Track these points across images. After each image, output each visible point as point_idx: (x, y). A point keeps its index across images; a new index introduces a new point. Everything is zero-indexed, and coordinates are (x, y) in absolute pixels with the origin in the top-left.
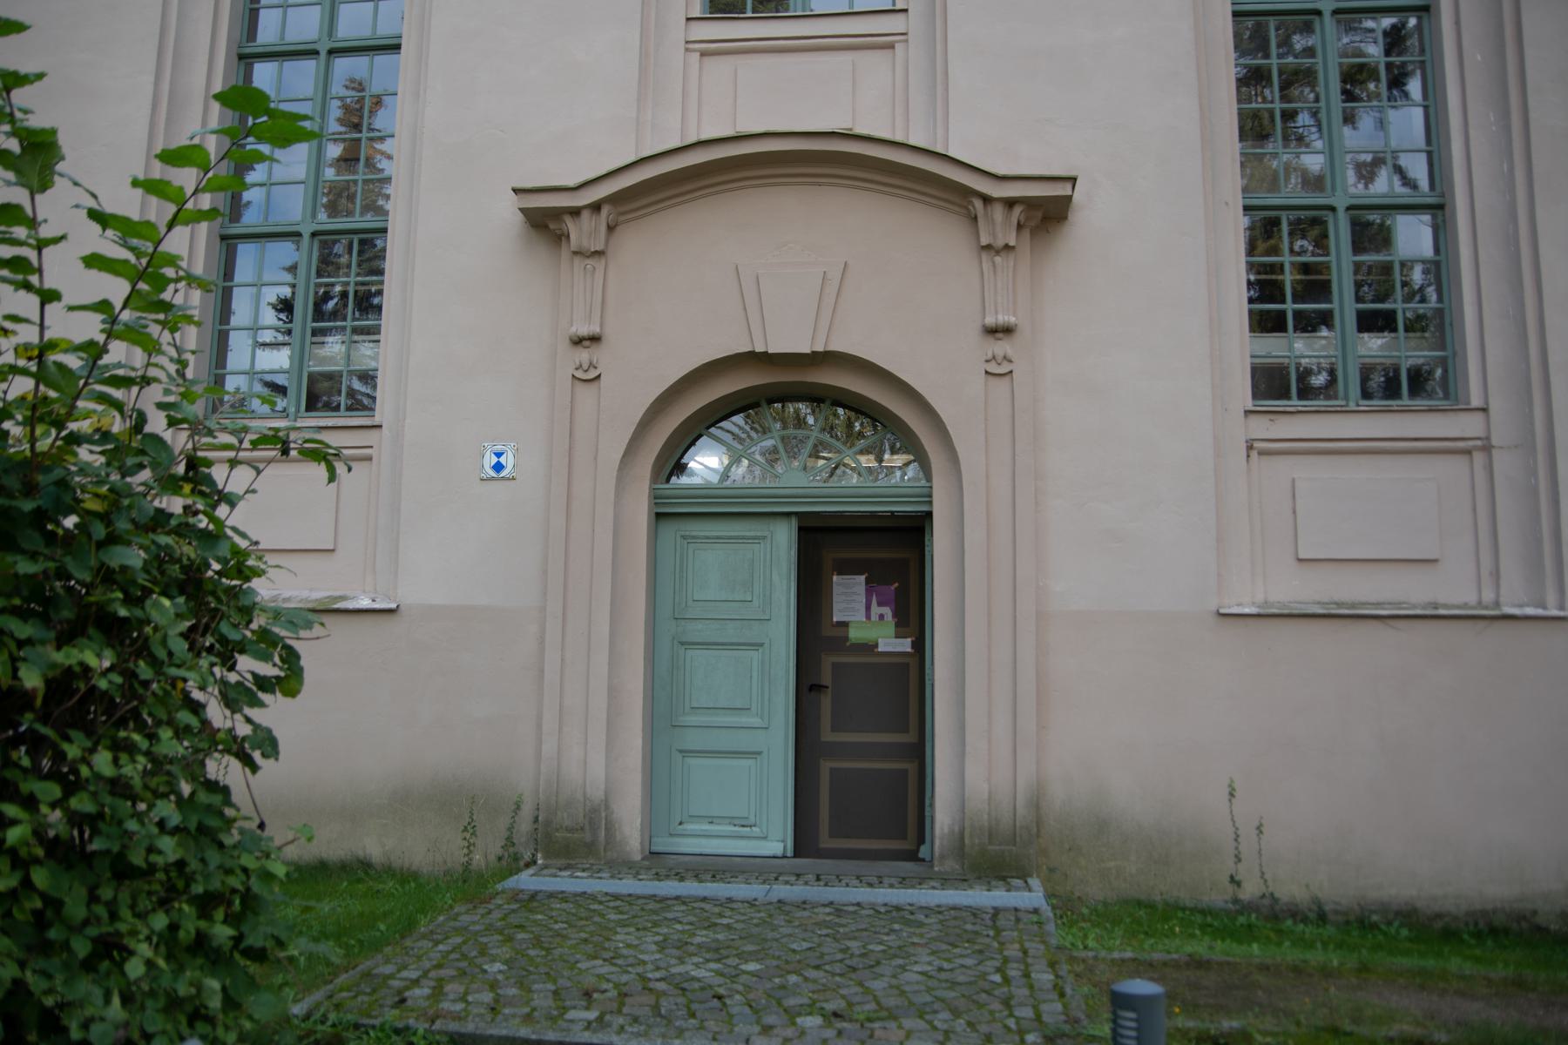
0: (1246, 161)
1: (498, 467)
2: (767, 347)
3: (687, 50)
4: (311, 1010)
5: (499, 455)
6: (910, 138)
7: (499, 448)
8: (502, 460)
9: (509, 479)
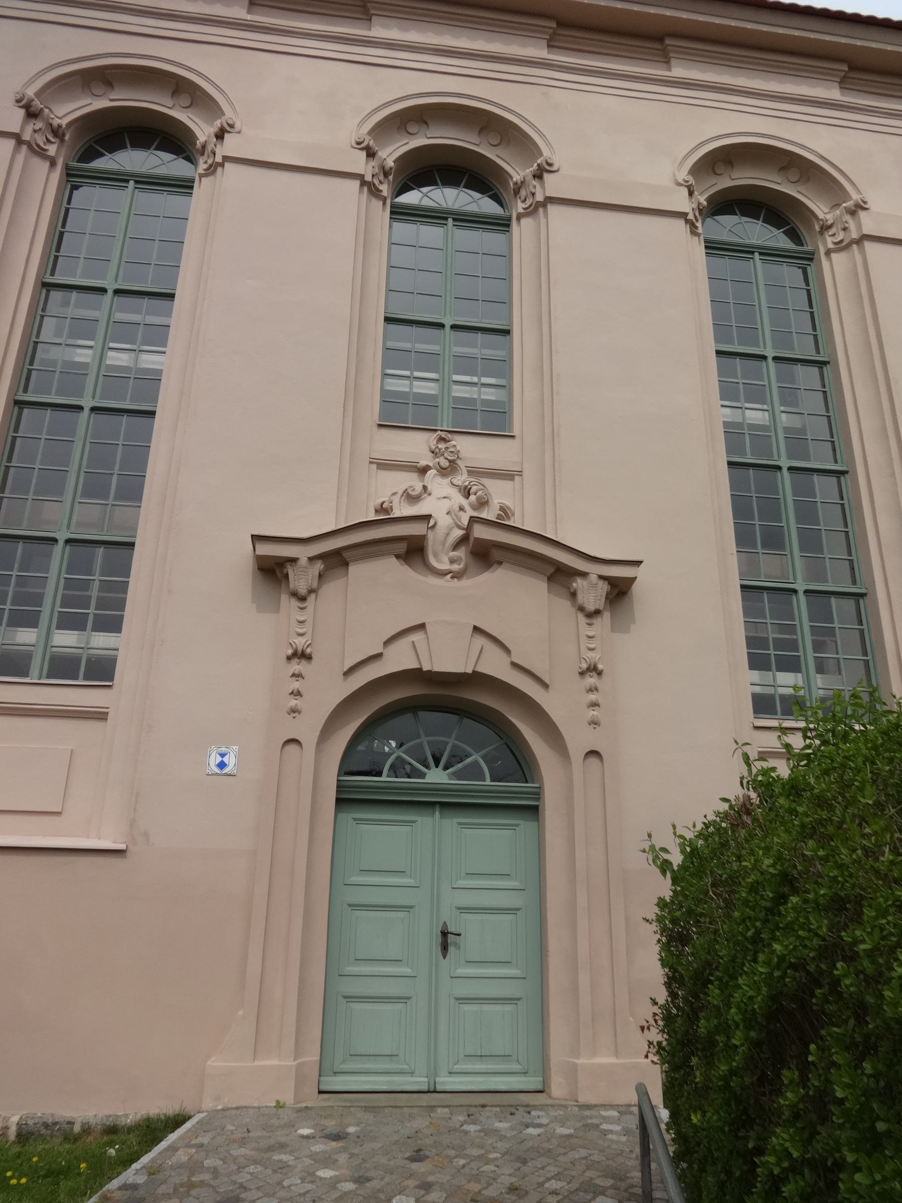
0: (747, 612)
1: (222, 765)
2: (420, 663)
3: (370, 463)
4: (299, 598)
5: (223, 755)
6: (434, 668)
7: (223, 750)
8: (226, 759)
9: (230, 775)
